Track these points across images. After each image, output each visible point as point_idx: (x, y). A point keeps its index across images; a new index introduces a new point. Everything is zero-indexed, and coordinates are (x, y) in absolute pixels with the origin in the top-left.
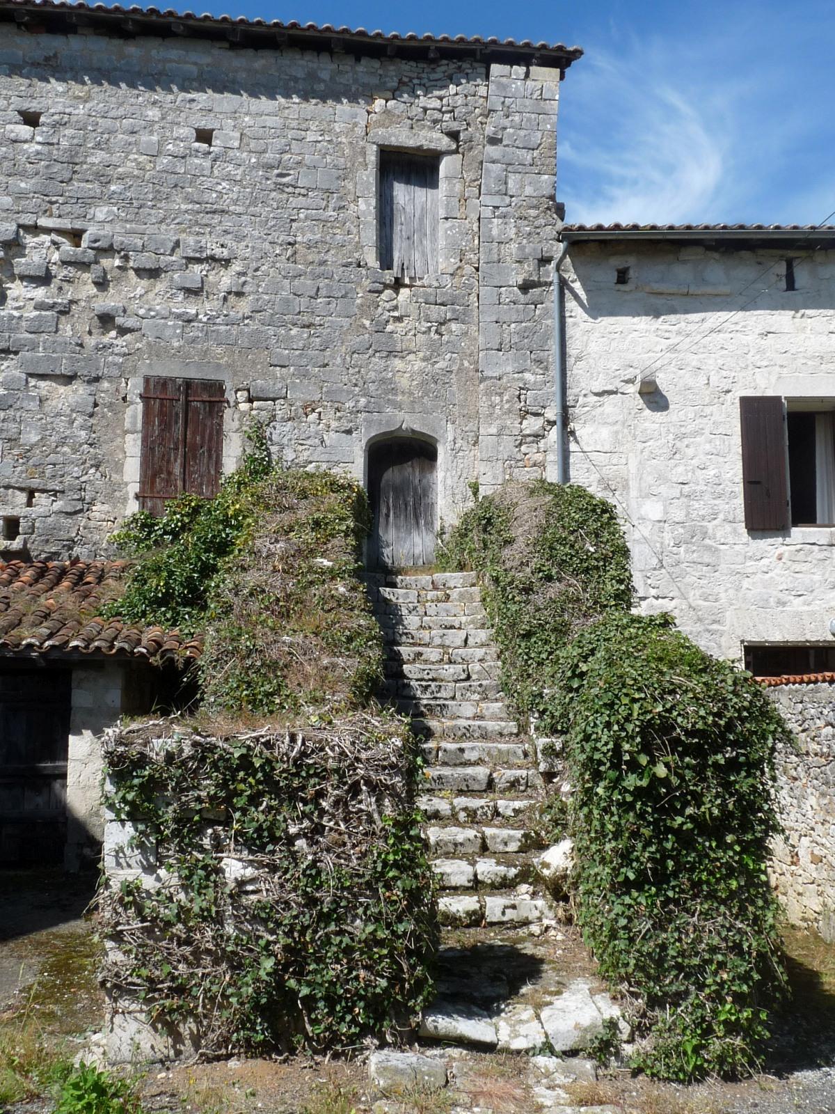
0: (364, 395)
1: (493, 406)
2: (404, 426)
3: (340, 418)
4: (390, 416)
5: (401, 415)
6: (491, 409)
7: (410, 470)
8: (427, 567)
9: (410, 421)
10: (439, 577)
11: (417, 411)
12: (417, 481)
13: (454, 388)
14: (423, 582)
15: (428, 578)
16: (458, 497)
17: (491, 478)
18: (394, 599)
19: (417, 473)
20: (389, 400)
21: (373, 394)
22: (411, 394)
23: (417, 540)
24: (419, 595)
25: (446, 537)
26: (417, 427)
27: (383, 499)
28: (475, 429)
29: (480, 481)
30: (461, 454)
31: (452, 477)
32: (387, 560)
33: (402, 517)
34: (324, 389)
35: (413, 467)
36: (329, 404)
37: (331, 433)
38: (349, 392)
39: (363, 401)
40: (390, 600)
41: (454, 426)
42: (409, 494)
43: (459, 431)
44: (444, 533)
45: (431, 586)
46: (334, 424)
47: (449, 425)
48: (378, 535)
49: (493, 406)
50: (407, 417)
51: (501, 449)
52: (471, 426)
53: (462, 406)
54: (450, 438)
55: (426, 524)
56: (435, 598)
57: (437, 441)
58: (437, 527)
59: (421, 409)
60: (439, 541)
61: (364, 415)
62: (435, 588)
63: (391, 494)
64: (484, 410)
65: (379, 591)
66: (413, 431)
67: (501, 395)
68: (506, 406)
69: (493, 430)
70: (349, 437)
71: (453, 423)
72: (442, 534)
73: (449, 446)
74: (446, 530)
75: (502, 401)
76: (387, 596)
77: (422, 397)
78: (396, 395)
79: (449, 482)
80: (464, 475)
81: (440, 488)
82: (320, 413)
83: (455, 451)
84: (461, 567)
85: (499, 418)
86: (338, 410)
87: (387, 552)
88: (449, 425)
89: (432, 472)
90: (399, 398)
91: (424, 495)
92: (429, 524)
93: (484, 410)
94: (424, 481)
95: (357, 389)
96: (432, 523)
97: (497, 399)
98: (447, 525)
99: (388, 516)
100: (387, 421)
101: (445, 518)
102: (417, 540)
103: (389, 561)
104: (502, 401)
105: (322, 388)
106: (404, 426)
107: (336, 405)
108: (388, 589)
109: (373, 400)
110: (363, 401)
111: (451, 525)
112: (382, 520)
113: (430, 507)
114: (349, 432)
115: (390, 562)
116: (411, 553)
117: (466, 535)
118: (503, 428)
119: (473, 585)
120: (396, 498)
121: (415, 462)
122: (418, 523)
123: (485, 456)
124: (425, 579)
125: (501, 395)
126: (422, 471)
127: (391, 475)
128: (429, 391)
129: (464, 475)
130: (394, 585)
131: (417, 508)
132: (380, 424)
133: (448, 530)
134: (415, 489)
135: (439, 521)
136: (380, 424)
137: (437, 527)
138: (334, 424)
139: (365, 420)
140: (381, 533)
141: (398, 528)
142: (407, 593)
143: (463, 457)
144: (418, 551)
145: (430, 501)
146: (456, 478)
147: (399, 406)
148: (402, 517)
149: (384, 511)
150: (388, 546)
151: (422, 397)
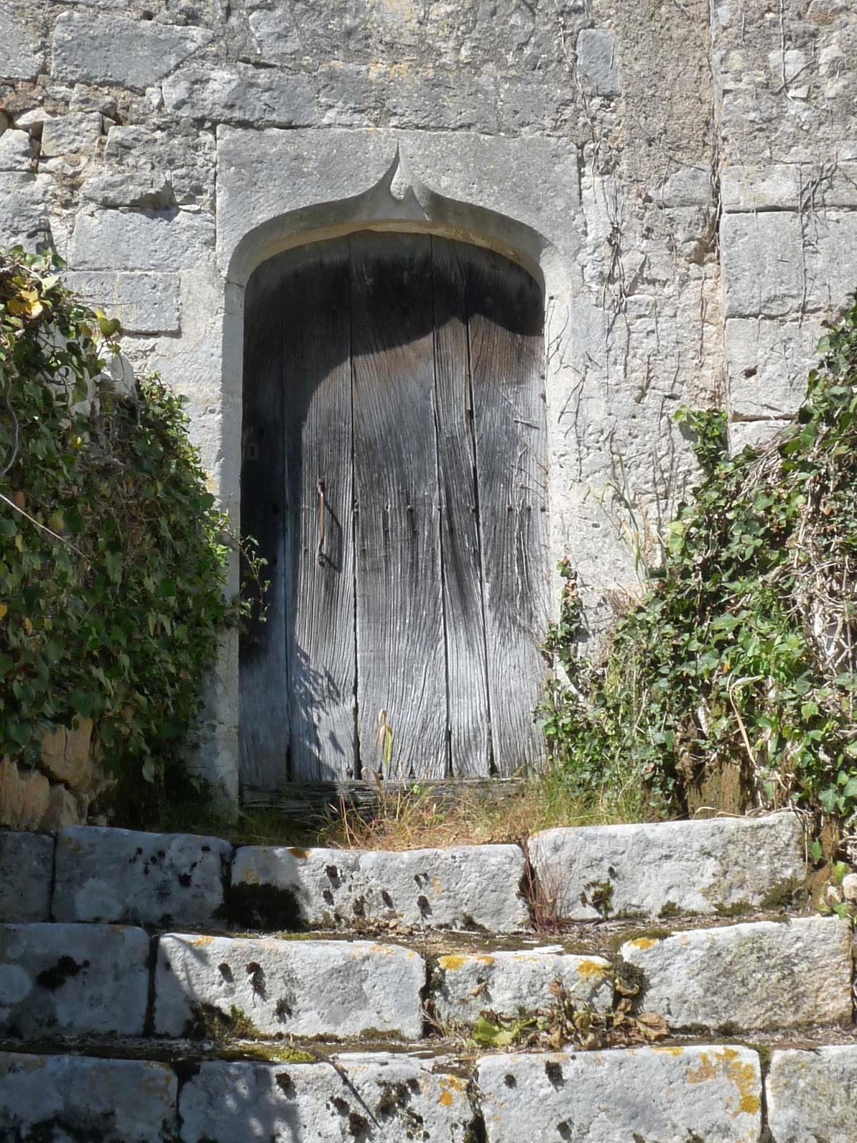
0: (228, 58)
1: (774, 89)
2: (398, 185)
3: (124, 148)
4: (338, 143)
5: (382, 139)
6: (767, 104)
7: (427, 369)
8: (492, 792)
9: (420, 163)
10: (566, 848)
11: (453, 119)
12: (457, 418)
13: (607, 32)
14: (470, 882)
15: (501, 856)
16: (640, 477)
17: (781, 385)
18: (260, 1015)
19: (459, 385)
20: (332, 75)
21: (268, 52)
22: (426, 51)
23: (465, 667)
24: (433, 985)
25: (591, 651)
26: (453, 187)
27: (310, 482)
28: (701, 193)
29: (729, 406)
30: (644, 295)
31: (611, 392)
32: (328, 756)
33: (396, 569)
34: (58, 32)
35: (439, 360)
36: (75, 94)
37: (82, 212)
38: (160, 46)
39: (222, 80)
40: (234, 1022)
41: (612, 182)
42: (422, 475)
43: (631, 201)
44: (580, 634)
45: (517, 913)
46: (95, 175)
47: (591, 179)
48: (291, 646)
49: (774, 89)
50: (410, 143)
51: (818, 263)
52: (685, 181)
53: (642, 103)
54: (598, 230)
55: (502, 596)
56: (542, 1002)
57: (537, 241)
58: (549, 607)
59: (466, 117)
60: (561, 670)
61: (226, 135)
62: (546, 922)
63: (348, 472)
64: (734, 102)
65: (155, 959)
66: (438, 204)
67: (807, 41)
68: (832, 88)
69: (782, 188)
70: (160, 226)
71: (608, 169)
72: (571, 637)
73: (593, 261)
74: (590, 620)
75: (812, 67)
76: (211, 990)
77: (474, 66)
78: (363, 55)
79: (596, 412)
80: (663, 384)
81: (557, 439)
82: (36, 133)
83: (621, 290)
84: (676, 790)
85: (803, 133)
86: (113, 115)
87: (330, 720)
88: (591, 179)
89: (520, 381)
90: (374, 71)
91: (490, 478)
92: (515, 600)
93: (734, 102)
94: (491, 418)
95: (197, 32)
96: (527, 595)
97: (793, 60)
98: (590, 600)
99: (333, 564)
100: (326, 162)
101: (583, 568)
102: (465, 667)
103: (338, 762)
104: (812, 67)
105: (46, 28)
106: (398, 185)
107: (106, 97)
108: (219, 946)
109: (263, 76)
110: (222, 80)
111: (612, 601)
112: (309, 582)
113: (520, 523)
114: (159, 205)
115: (346, 763)
116: (438, 724)
117: (714, 603)
118: (825, 176)
119: (785, 900)
120: (371, 487)
121: (452, 336)
122: (463, 594)
123: (749, 294)
124: (477, 865)
125: (807, 41)
126: (480, 372)
127: (351, 394)
128: (504, 40)
129: (663, 384)
130: (276, 910)
131: (467, 537)
132: (296, 173)
133: (599, 620)
134: (451, 451)
135: (559, 583)
136: (296, 173)
137: (549, 607)
138: (95, 175)
139: (230, 157)
140: (303, 640)
141: (378, 617)
142: (348, 971)
143: (655, 309)
144: (465, 715)
145: (515, 500)
146: (626, 399)
147: (376, 104)
148: (396, 569)
149: (315, 540)
150: (334, 694)
151: (474, 66)
